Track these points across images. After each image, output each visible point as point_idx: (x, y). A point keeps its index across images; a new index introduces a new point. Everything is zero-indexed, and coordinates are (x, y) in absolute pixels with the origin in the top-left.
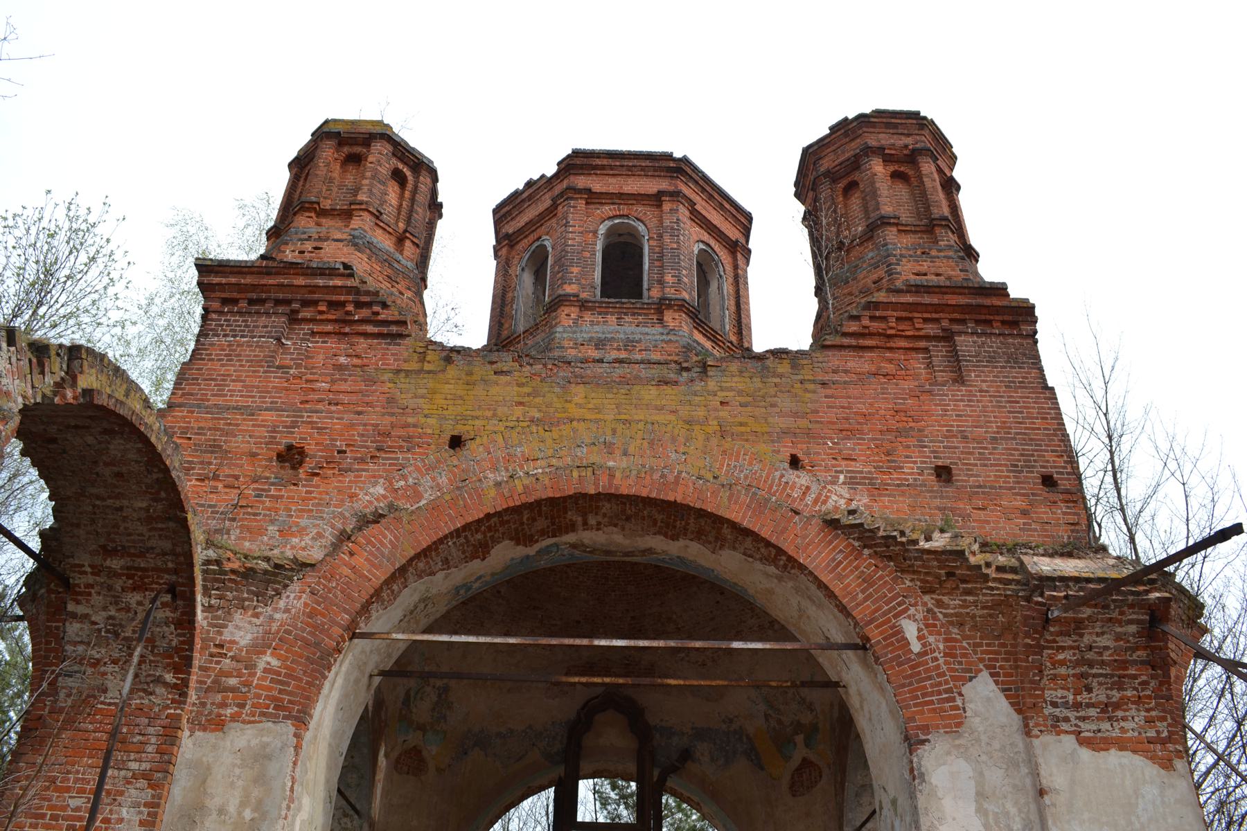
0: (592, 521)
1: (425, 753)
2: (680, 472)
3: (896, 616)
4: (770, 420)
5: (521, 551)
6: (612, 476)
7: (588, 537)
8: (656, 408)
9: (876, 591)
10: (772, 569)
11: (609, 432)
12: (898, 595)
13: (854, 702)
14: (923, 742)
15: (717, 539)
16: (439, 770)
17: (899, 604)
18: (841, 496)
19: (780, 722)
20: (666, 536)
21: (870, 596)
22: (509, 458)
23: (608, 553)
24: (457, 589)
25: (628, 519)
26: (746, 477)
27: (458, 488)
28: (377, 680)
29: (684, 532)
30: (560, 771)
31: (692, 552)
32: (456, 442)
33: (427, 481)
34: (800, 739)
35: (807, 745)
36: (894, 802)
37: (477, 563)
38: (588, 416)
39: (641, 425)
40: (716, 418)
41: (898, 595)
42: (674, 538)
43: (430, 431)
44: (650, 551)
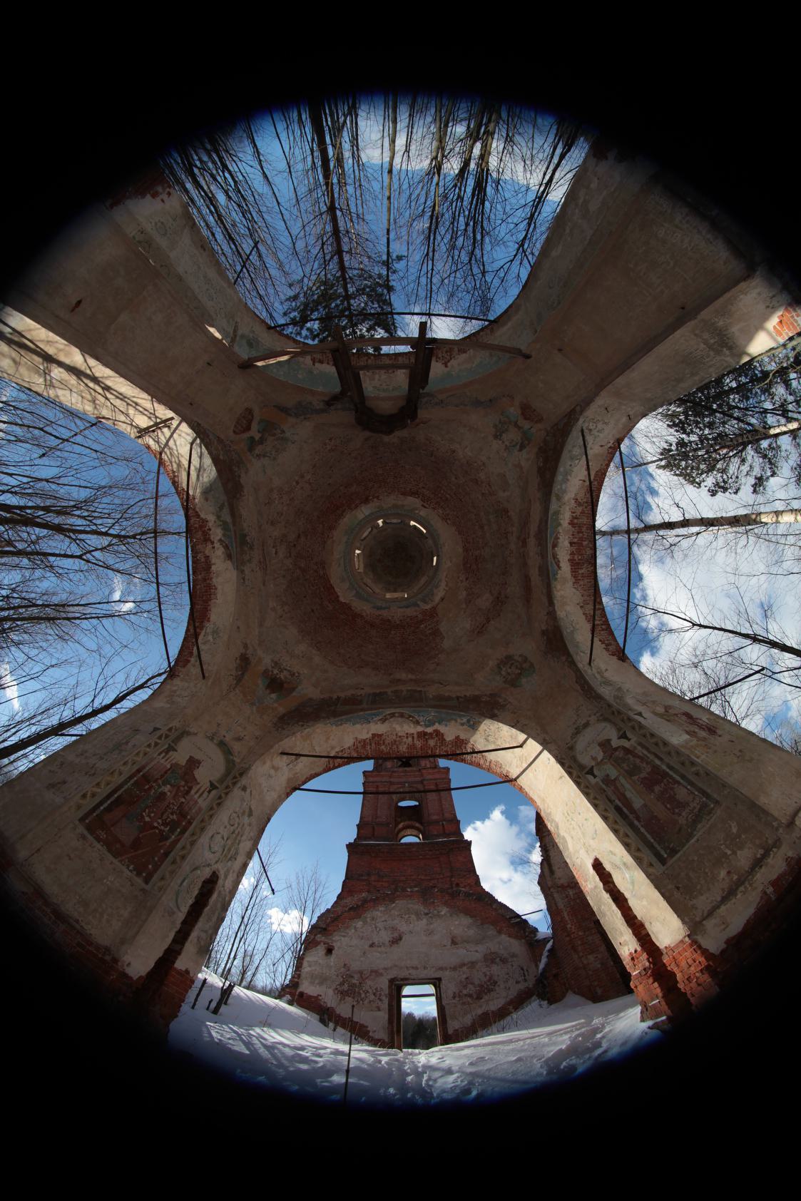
5: (442, 729)
19: (274, 435)
23: (402, 715)
34: (257, 437)
42: (374, 735)
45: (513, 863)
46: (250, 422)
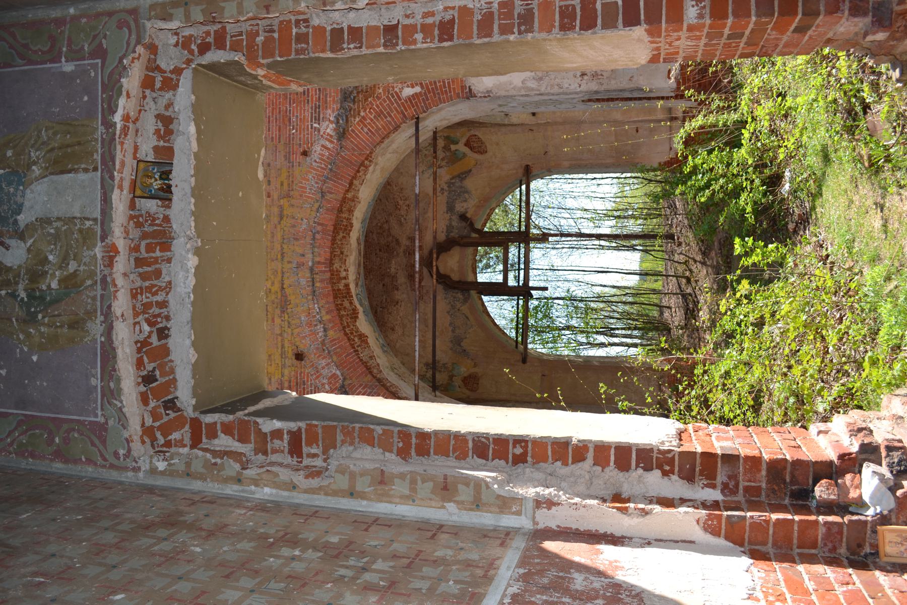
0: (343, 274)
1: (466, 375)
2: (315, 222)
3: (400, 100)
4: (278, 167)
5: (361, 316)
6: (319, 263)
7: (352, 277)
8: (273, 237)
9: (386, 110)
10: (371, 169)
11: (290, 266)
12: (388, 97)
13: (445, 123)
14: (470, 90)
15: (353, 201)
16: (475, 365)
17: (393, 97)
18: (328, 126)
20: (350, 231)
21: (388, 113)
22: (310, 325)
23: (359, 265)
24: (384, 352)
25: (342, 253)
26: (317, 183)
27: (329, 352)
28: (438, 393)
29: (349, 219)
30: (473, 293)
31: (359, 215)
32: (299, 357)
33: (325, 372)
34: (453, 147)
35: (457, 143)
36: (500, 106)
37: (369, 340)
38: (279, 278)
39: (285, 246)
40: (279, 199)
41: (388, 97)
42: (351, 225)
43: (293, 373)
44: (358, 240)
45: (527, 166)
46: (471, 148)
